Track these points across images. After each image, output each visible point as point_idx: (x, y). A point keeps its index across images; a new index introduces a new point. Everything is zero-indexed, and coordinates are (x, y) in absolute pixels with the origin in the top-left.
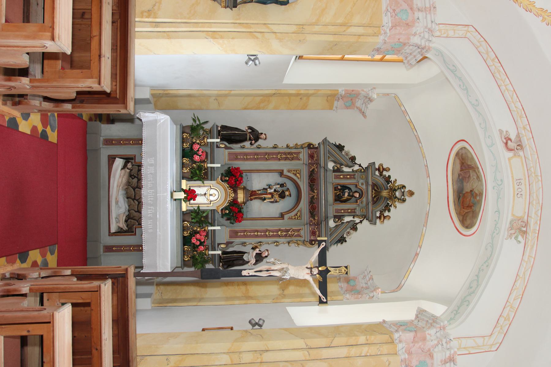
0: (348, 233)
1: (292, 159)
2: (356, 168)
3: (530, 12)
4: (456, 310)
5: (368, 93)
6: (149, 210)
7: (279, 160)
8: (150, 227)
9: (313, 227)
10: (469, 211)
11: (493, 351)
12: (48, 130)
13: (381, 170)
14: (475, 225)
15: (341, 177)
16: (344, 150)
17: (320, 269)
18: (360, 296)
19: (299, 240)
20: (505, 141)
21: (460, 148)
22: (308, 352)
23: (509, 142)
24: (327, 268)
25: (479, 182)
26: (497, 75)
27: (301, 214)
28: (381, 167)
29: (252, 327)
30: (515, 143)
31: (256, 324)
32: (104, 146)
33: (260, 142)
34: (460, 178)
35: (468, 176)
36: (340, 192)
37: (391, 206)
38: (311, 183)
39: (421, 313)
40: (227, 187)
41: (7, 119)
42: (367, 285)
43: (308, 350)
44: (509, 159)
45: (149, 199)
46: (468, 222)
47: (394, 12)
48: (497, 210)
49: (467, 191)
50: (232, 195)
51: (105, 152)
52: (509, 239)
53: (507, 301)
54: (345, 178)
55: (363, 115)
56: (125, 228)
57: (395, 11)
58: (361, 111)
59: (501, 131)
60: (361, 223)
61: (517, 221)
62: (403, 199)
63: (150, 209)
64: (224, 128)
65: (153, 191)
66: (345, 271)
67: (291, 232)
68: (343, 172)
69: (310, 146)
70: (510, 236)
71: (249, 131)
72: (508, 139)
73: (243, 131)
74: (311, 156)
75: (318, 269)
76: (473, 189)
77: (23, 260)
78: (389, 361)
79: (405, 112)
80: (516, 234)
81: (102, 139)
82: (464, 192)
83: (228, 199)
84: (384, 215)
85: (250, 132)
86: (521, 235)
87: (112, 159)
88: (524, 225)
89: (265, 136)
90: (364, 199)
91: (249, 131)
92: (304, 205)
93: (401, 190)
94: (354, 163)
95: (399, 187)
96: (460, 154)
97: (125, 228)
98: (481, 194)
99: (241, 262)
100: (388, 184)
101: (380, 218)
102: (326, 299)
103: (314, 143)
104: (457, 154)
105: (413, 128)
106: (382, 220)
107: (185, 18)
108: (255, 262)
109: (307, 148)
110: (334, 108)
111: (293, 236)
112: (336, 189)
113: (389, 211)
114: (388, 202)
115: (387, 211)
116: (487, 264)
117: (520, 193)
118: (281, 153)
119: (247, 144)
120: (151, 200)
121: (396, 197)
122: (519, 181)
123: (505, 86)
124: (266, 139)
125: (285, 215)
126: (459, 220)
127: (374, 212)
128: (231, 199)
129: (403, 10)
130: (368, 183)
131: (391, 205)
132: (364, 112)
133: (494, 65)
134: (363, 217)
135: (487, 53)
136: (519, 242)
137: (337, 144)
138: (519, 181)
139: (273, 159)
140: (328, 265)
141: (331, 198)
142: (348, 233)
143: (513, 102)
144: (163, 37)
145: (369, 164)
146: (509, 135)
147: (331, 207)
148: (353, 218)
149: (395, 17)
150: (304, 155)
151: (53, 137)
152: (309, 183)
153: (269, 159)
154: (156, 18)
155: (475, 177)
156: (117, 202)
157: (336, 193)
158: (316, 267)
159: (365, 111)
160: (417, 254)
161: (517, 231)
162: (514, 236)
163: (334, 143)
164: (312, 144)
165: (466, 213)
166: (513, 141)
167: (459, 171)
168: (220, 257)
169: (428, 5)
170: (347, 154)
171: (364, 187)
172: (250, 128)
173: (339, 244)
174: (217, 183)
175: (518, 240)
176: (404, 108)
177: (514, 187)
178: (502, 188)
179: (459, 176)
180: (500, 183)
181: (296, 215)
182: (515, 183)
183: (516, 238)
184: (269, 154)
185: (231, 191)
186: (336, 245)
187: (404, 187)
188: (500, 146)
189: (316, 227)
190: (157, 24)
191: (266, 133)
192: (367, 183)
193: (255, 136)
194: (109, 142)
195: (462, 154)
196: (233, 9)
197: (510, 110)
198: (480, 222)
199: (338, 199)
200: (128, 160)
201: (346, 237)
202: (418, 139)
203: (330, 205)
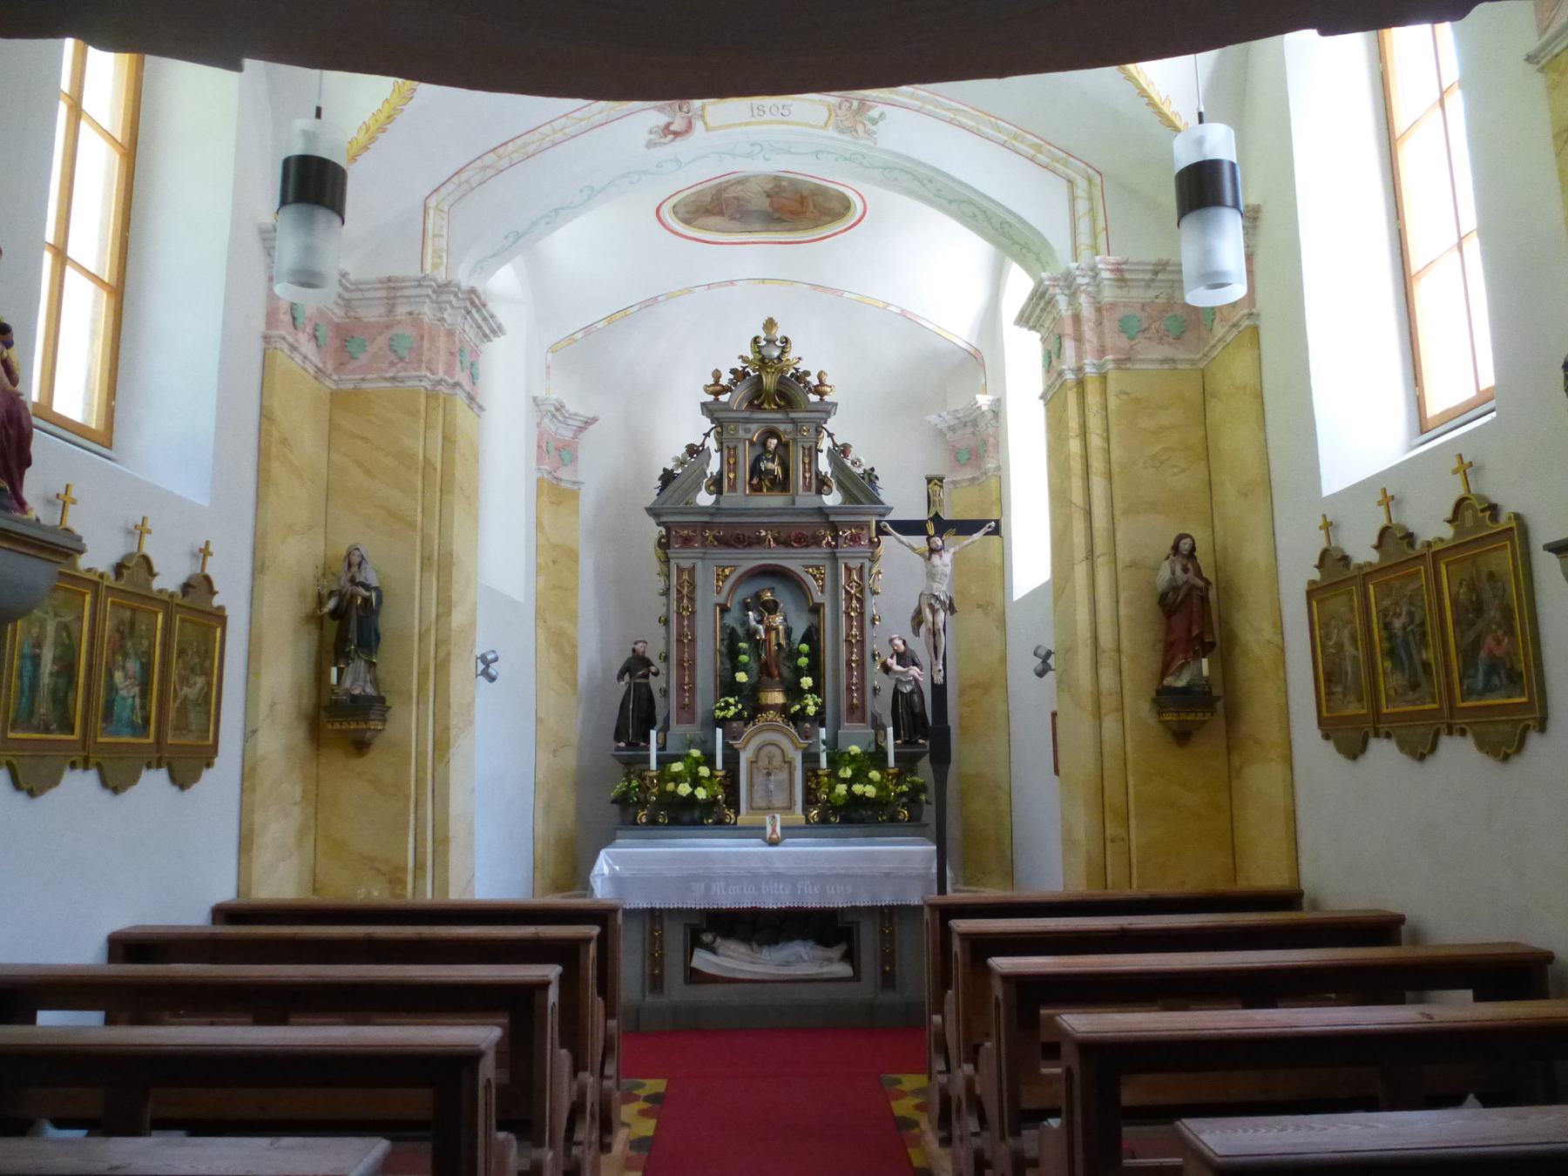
0: (854, 463)
1: (692, 585)
2: (712, 443)
3: (413, 92)
4: (1021, 249)
5: (544, 413)
6: (806, 892)
7: (693, 613)
8: (842, 890)
9: (841, 541)
10: (811, 203)
11: (1102, 181)
12: (643, 1093)
13: (717, 389)
14: (843, 194)
15: (732, 476)
16: (672, 470)
17: (932, 532)
18: (991, 440)
19: (870, 570)
20: (671, 137)
21: (673, 216)
22: (1099, 557)
23: (672, 128)
24: (931, 519)
25: (751, 180)
26: (531, 149)
27: (812, 567)
28: (711, 389)
29: (1050, 672)
30: (675, 115)
31: (1044, 661)
32: (666, 992)
33: (653, 653)
34: (738, 216)
35: (736, 202)
36: (764, 480)
37: (797, 370)
38: (746, 543)
39: (1025, 319)
40: (754, 725)
41: (633, 1153)
42: (969, 424)
43: (1095, 558)
44: (708, 129)
45: (782, 892)
46: (835, 205)
47: (396, 363)
48: (815, 156)
49: (767, 204)
50: (771, 716)
51: (677, 991)
52: (875, 136)
53: (1003, 145)
54: (734, 467)
55: (591, 424)
56: (842, 948)
57: (392, 362)
58: (581, 427)
59: (650, 145)
60: (833, 434)
61: (839, 118)
62: (782, 343)
63: (802, 890)
64: (619, 735)
65: (763, 884)
66: (936, 484)
67: (851, 587)
68: (721, 473)
69: (664, 545)
70: (869, 134)
71: (627, 677)
72: (666, 130)
73: (629, 689)
74: (687, 542)
75: (934, 536)
76: (765, 192)
77: (915, 1124)
78: (1120, 393)
79: (588, 330)
80: (865, 122)
81: (649, 999)
82: (771, 210)
83: (781, 724)
84: (818, 386)
85: (631, 677)
86: (868, 110)
87: (695, 977)
88: (848, 105)
89: (641, 644)
90: (781, 427)
91: (627, 677)
92: (794, 561)
93: (762, 347)
94: (701, 448)
95: (757, 350)
96: (687, 216)
97: (842, 948)
98: (777, 178)
99: (916, 698)
100: (748, 374)
101: (822, 394)
102: (990, 521)
103: (656, 536)
104: (687, 222)
105: (623, 314)
106: (829, 389)
107: (407, 806)
108: (915, 668)
109: (667, 551)
110: (576, 487)
111: (860, 585)
112: (756, 489)
113: (807, 373)
114: (788, 375)
115: (808, 379)
116: (925, 182)
117: (781, 110)
118: (678, 608)
119: (656, 684)
120: (784, 889)
121: (779, 358)
122: (755, 111)
123: (555, 132)
124: (645, 642)
125: (815, 601)
126: (830, 222)
127: (810, 408)
128: (781, 717)
129: (391, 346)
130: (746, 418)
131: (794, 368)
132: (586, 422)
133: (509, 155)
134: (821, 432)
135: (485, 168)
136: (882, 115)
137: (659, 484)
138: (755, 111)
139: (692, 627)
140: (926, 518)
141: (776, 500)
142: (854, 463)
143: (589, 118)
144: (446, 853)
145: (703, 414)
146: (658, 126)
147: (798, 499)
148: (821, 451)
149: (407, 363)
150: (683, 558)
151: (656, 1085)
152: (744, 547)
153: (693, 634)
154: (406, 868)
155: (739, 188)
156: (787, 964)
157: (769, 490)
158: (928, 540)
159: (582, 419)
160: (903, 314)
161: (858, 118)
162: (869, 126)
163: (658, 491)
164: (660, 539)
165: (815, 206)
166: (671, 120)
167: (722, 218)
168: (905, 743)
169: (383, 294)
170: (681, 463)
171: (754, 427)
172: (621, 677)
173: (878, 483)
174: (745, 746)
175: (877, 117)
176: (578, 332)
177: (766, 123)
178: (770, 145)
179: (735, 219)
180: (757, 148)
181: (814, 576)
182: (759, 118)
183: (874, 122)
184: (680, 635)
185: (762, 716)
186: (880, 491)
187: (756, 340)
188: (681, 145)
189: (841, 533)
190: (419, 866)
191: (499, 660)
192: (748, 421)
193: (637, 665)
194: (656, 982)
195: (688, 212)
196: (388, 704)
197: (606, 123)
198: (837, 183)
199: (782, 484)
200: (694, 941)
201: (863, 468)
202: (651, 302)
203: (793, 502)
